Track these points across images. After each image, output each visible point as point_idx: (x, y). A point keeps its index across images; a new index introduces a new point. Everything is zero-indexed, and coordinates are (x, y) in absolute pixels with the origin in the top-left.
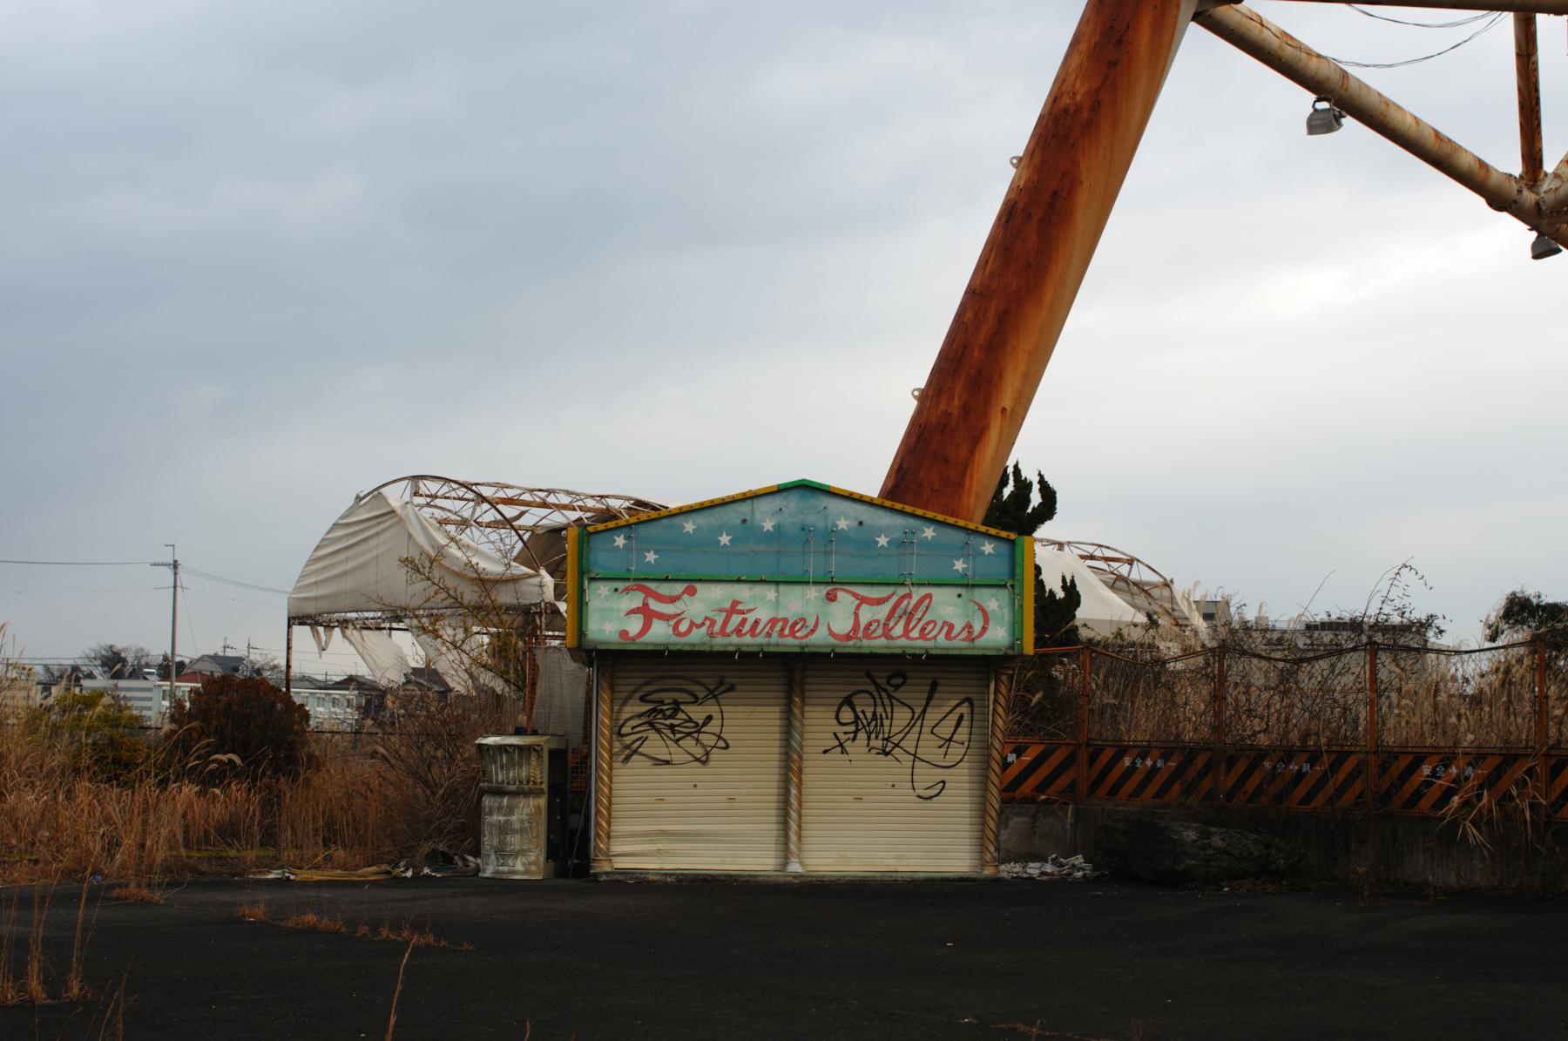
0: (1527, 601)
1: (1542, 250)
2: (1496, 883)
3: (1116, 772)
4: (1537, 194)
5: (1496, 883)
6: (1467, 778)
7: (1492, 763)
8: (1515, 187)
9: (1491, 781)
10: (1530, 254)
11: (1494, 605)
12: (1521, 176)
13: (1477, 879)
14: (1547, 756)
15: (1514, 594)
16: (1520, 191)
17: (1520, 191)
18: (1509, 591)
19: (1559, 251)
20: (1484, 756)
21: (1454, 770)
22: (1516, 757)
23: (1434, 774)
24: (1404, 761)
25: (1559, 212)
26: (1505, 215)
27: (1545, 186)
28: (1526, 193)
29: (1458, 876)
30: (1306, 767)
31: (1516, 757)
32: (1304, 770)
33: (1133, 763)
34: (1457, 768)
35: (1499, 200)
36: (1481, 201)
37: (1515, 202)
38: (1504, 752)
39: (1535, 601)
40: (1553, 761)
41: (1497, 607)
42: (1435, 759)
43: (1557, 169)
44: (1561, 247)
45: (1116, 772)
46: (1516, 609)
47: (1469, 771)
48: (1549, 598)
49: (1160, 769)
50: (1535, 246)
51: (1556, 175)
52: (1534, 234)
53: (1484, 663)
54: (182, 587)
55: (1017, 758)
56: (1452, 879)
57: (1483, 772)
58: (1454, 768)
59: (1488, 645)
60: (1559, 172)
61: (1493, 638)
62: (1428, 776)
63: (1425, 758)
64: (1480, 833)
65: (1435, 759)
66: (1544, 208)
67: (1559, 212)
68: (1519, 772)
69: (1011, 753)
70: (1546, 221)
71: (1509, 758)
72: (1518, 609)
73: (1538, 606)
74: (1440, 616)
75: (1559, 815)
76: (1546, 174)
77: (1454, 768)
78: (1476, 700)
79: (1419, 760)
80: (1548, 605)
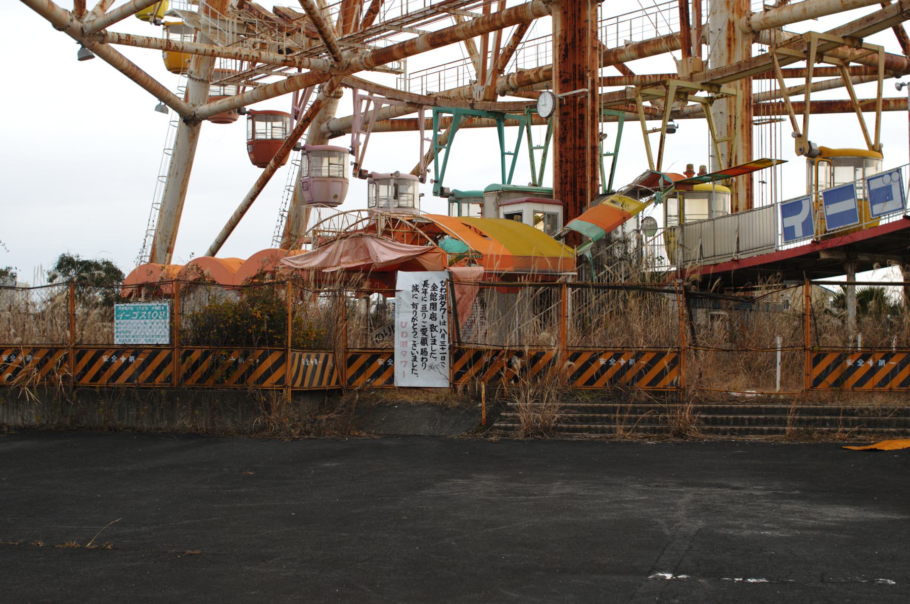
0: (72, 259)
1: (82, 56)
2: (45, 422)
3: (594, 369)
4: (82, 23)
5: (45, 422)
6: (27, 362)
7: (43, 353)
8: (69, 17)
9: (40, 366)
10: (77, 58)
11: (51, 264)
12: (73, 12)
13: (34, 420)
14: (75, 348)
15: (63, 255)
16: (72, 20)
17: (72, 20)
18: (60, 254)
19: (93, 57)
20: (38, 349)
21: (20, 358)
22: (57, 349)
23: (9, 361)
24: (90, 354)
25: (94, 34)
26: (63, 33)
27: (86, 19)
28: (75, 21)
29: (23, 419)
30: (132, 359)
31: (57, 349)
32: (630, 363)
33: (110, 359)
34: (874, 360)
35: (59, 25)
36: (49, 24)
37: (69, 26)
38: (50, 346)
39: (75, 259)
40: (78, 351)
41: (54, 262)
42: (9, 352)
43: (94, 9)
44: (95, 55)
45: (594, 369)
46: (64, 263)
47: (29, 358)
48: (83, 258)
49: (131, 363)
50: (80, 53)
51: (94, 13)
52: (80, 46)
53: (44, 294)
54: (618, 23)
55: (886, 363)
56: (19, 421)
57: (38, 358)
58: (871, 360)
59: (49, 284)
60: (96, 11)
61: (51, 280)
62: (5, 362)
63: (105, 351)
64: (33, 393)
65: (9, 352)
66: (85, 31)
67: (94, 34)
68: (58, 357)
69: (881, 359)
70: (86, 39)
71: (52, 351)
72: (66, 263)
73: (78, 262)
74: (14, 268)
75: (81, 382)
76: (87, 12)
77: (871, 360)
78: (40, 316)
79: (100, 353)
80: (84, 262)
